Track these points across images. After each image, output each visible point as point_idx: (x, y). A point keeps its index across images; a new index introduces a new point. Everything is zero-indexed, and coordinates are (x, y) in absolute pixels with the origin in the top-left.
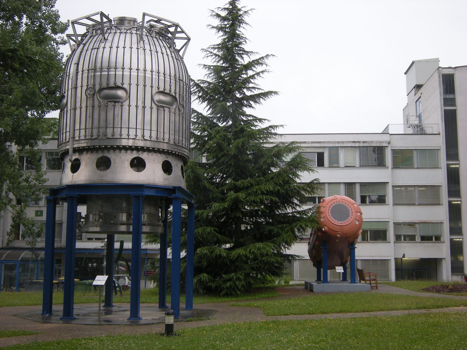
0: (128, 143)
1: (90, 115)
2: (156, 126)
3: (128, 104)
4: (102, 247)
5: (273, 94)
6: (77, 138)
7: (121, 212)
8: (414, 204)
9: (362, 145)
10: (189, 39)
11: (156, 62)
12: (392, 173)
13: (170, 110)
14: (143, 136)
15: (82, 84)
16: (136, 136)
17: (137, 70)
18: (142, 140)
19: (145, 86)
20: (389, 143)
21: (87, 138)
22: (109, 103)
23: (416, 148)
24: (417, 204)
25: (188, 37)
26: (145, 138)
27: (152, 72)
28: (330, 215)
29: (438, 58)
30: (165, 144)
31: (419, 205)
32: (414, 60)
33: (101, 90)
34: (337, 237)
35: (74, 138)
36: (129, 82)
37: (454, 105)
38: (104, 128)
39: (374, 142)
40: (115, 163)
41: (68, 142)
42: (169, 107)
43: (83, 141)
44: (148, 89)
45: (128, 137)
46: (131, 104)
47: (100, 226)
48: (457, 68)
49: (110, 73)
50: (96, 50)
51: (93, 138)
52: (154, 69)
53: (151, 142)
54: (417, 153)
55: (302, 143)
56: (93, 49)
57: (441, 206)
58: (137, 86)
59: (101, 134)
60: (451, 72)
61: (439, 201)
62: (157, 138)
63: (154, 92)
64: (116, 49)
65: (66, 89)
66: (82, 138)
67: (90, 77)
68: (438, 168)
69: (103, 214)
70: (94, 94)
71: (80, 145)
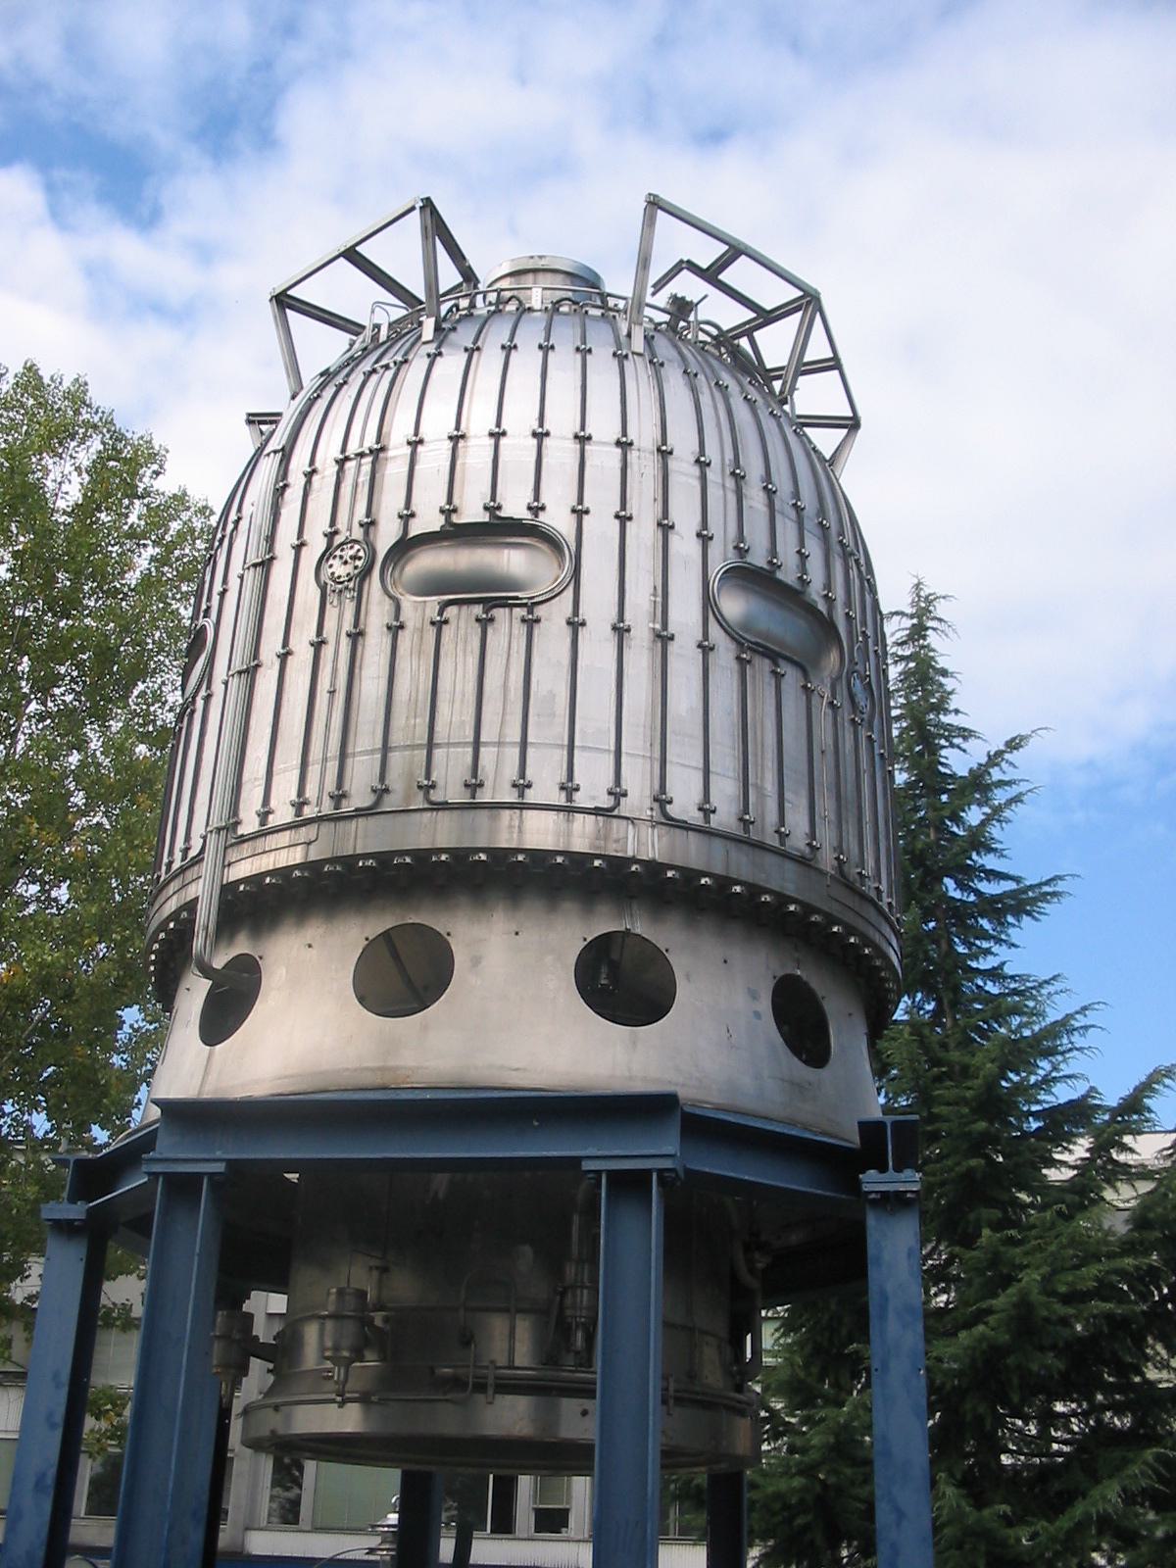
0: (569, 834)
1: (333, 683)
2: (738, 753)
3: (569, 611)
4: (371, 1551)
6: (249, 824)
7: (507, 1310)
14: (661, 800)
15: (286, 643)
16: (618, 794)
17: (618, 443)
18: (654, 824)
19: (665, 528)
21: (309, 812)
22: (451, 612)
30: (789, 866)
33: (405, 546)
38: (419, 746)
40: (476, 961)
41: (198, 860)
43: (284, 838)
44: (684, 545)
45: (570, 799)
46: (585, 612)
47: (364, 1399)
51: (348, 807)
52: (712, 453)
56: (347, 459)
59: (395, 780)
62: (746, 824)
63: (717, 567)
66: (283, 814)
69: (386, 1320)
70: (366, 572)
71: (266, 863)
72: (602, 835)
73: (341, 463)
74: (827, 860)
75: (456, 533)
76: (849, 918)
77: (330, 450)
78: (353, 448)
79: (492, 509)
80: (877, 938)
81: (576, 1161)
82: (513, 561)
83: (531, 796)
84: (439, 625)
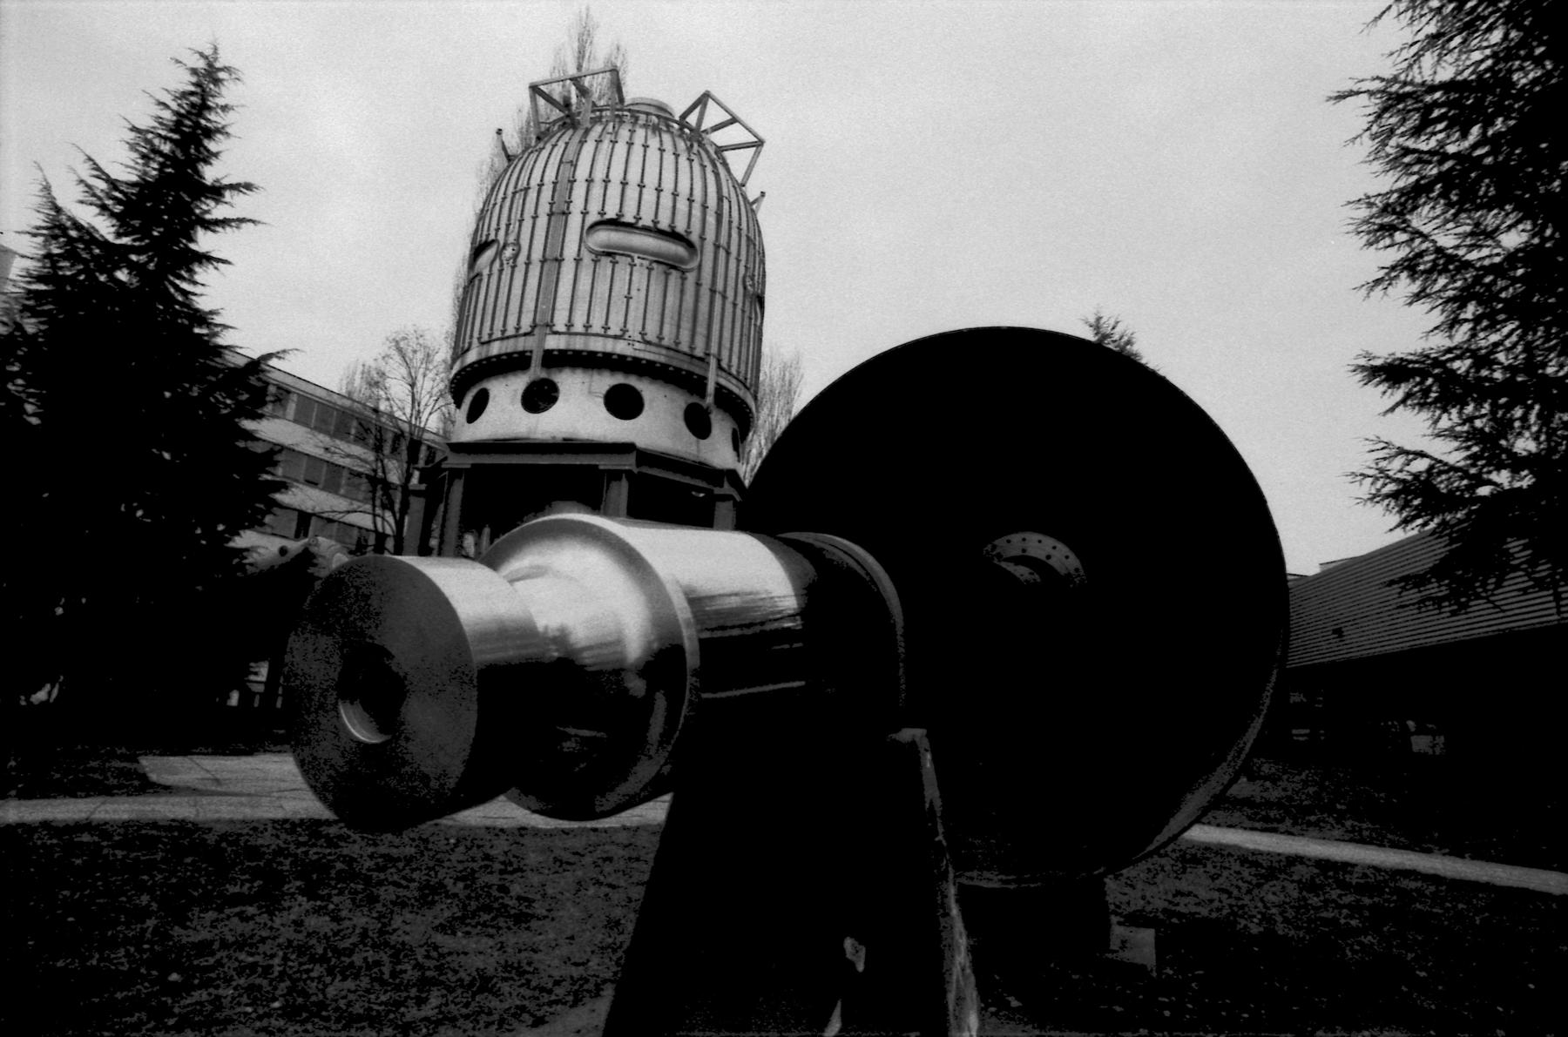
10: (759, 144)
14: (643, 334)
26: (648, 338)
45: (568, 329)
50: (523, 193)
51: (522, 331)
64: (642, 149)
66: (497, 334)
72: (586, 343)
73: (514, 193)
75: (616, 223)
77: (511, 189)
78: (519, 187)
79: (655, 222)
81: (597, 466)
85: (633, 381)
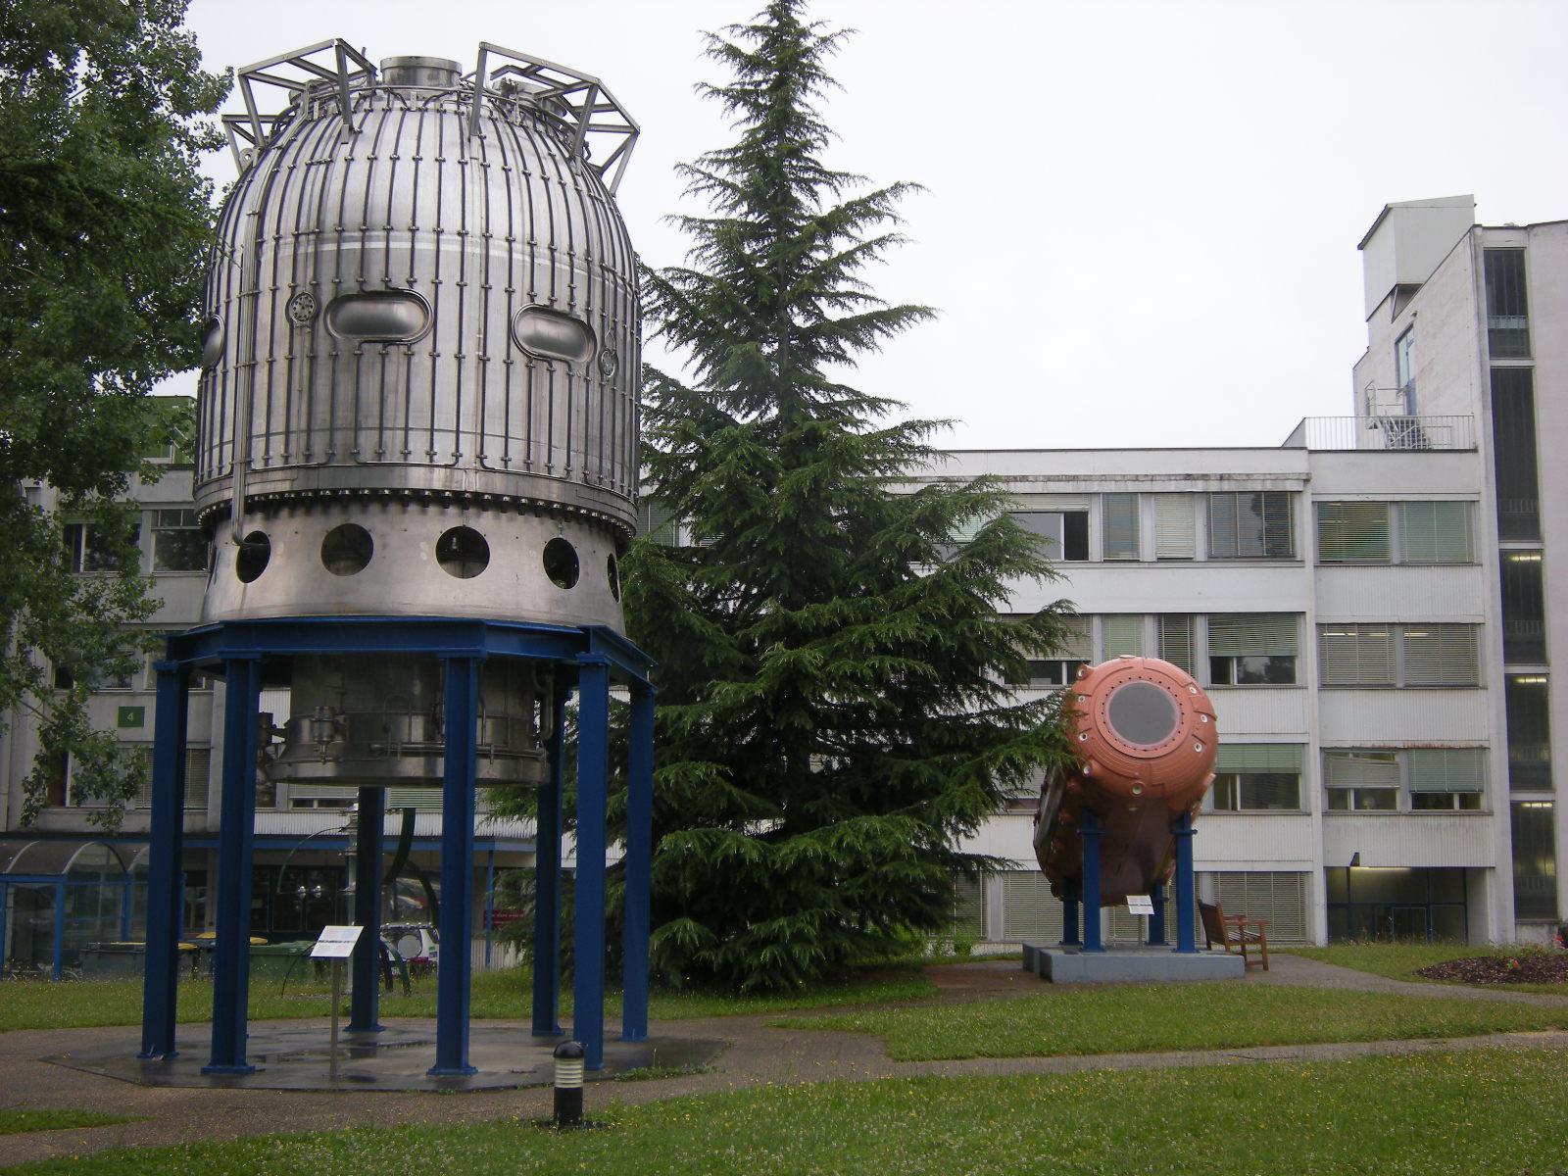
0: (431, 480)
1: (301, 385)
2: (525, 424)
3: (430, 348)
5: (917, 317)
6: (258, 465)
7: (407, 714)
8: (1390, 687)
9: (1214, 486)
10: (634, 132)
11: (522, 208)
12: (1318, 581)
13: (570, 370)
14: (481, 457)
15: (274, 284)
16: (457, 455)
17: (459, 234)
18: (477, 471)
19: (486, 288)
20: (1306, 481)
21: (293, 462)
22: (365, 346)
23: (1398, 498)
24: (1400, 685)
25: (632, 126)
26: (488, 463)
27: (510, 241)
28: (1108, 721)
29: (1472, 196)
30: (555, 484)
31: (1408, 687)
32: (1391, 200)
33: (339, 301)
34: (1131, 798)
35: (250, 462)
36: (433, 277)
37: (1525, 351)
38: (350, 429)
39: (1255, 477)
40: (385, 546)
41: (230, 476)
42: (568, 358)
43: (279, 475)
44: (498, 298)
45: (431, 461)
46: (440, 348)
47: (336, 760)
48: (1535, 230)
49: (368, 245)
50: (323, 168)
51: (314, 463)
52: (517, 231)
53: (505, 476)
54: (1400, 514)
55: (1015, 479)
57: (1481, 693)
58: (458, 288)
59: (339, 451)
60: (1513, 241)
61: (1476, 676)
62: (528, 465)
63: (517, 308)
64: (390, 163)
65: (223, 298)
66: (277, 462)
67: (301, 259)
68: (1470, 564)
69: (345, 720)
70: (315, 317)
71: (270, 488)
74: (577, 477)
76: (598, 507)
80: (614, 514)
82: (403, 312)
83: (411, 460)
84: (359, 357)
85: (572, 535)
